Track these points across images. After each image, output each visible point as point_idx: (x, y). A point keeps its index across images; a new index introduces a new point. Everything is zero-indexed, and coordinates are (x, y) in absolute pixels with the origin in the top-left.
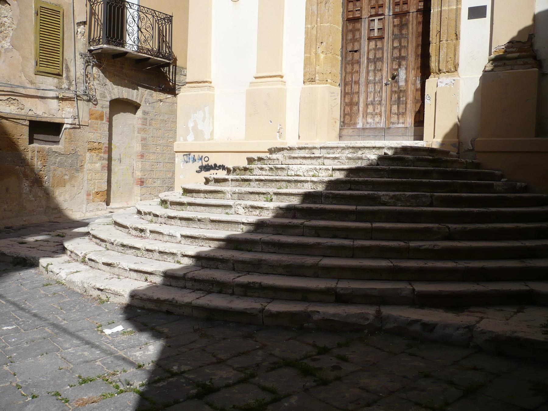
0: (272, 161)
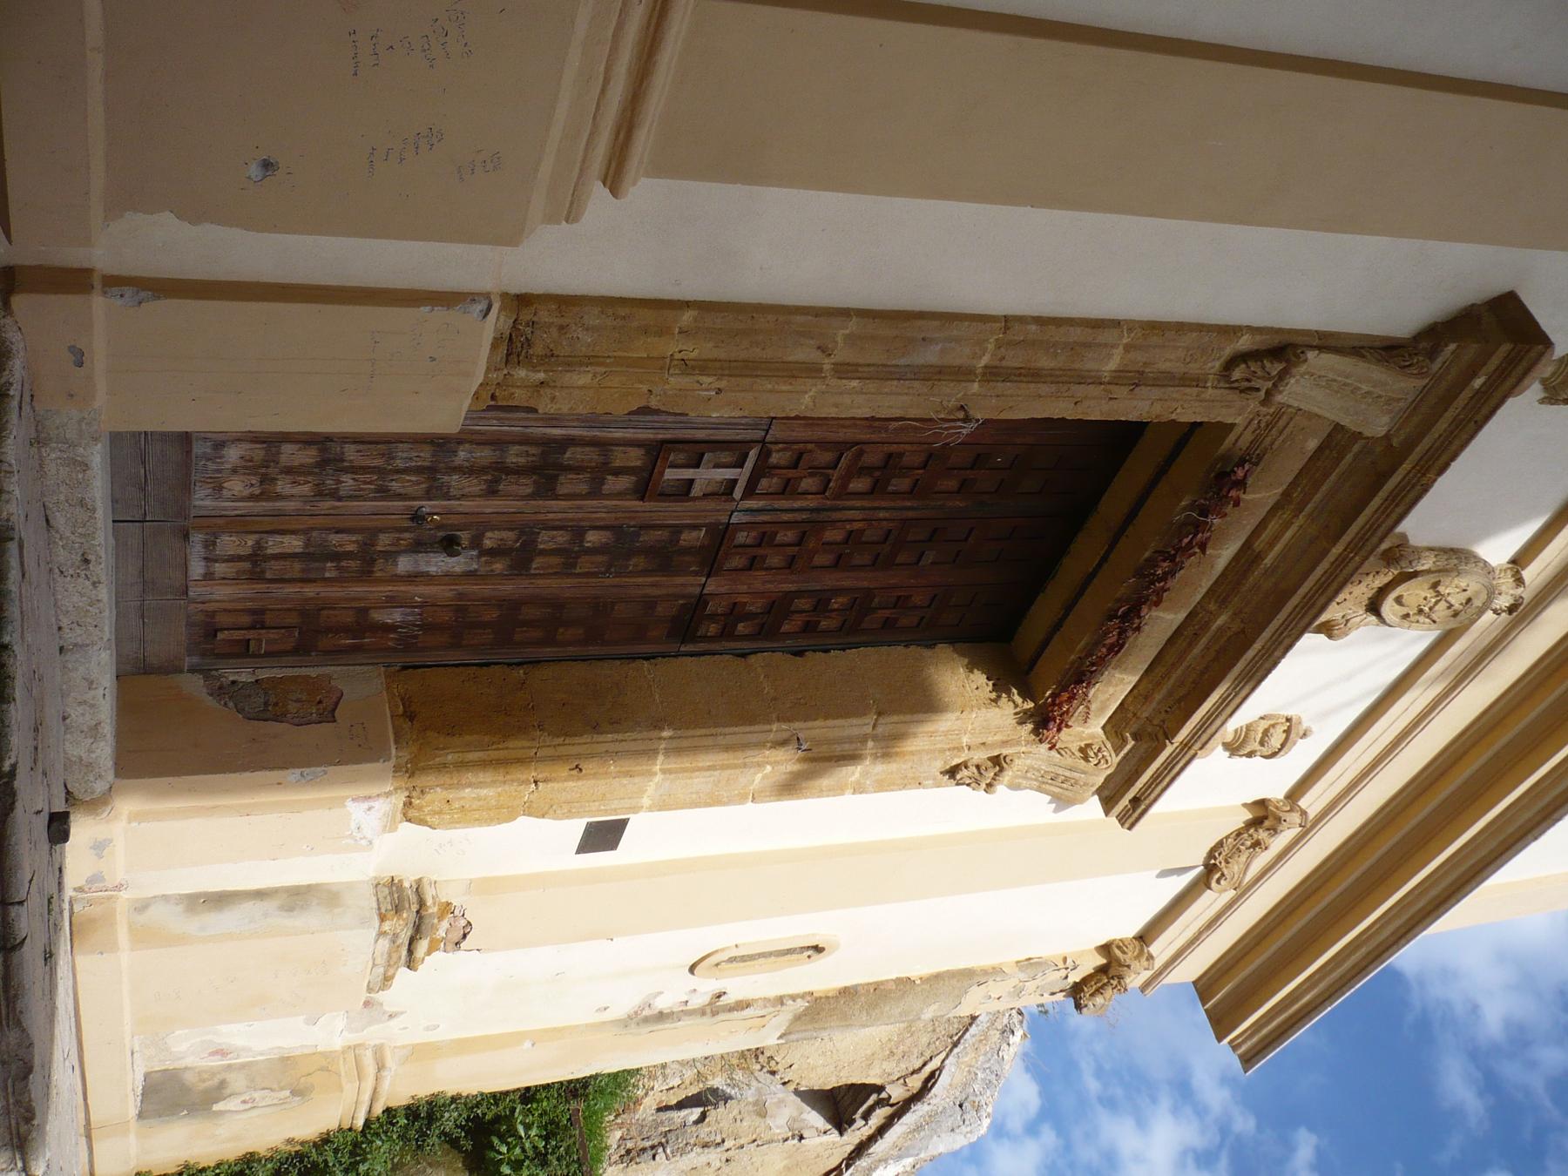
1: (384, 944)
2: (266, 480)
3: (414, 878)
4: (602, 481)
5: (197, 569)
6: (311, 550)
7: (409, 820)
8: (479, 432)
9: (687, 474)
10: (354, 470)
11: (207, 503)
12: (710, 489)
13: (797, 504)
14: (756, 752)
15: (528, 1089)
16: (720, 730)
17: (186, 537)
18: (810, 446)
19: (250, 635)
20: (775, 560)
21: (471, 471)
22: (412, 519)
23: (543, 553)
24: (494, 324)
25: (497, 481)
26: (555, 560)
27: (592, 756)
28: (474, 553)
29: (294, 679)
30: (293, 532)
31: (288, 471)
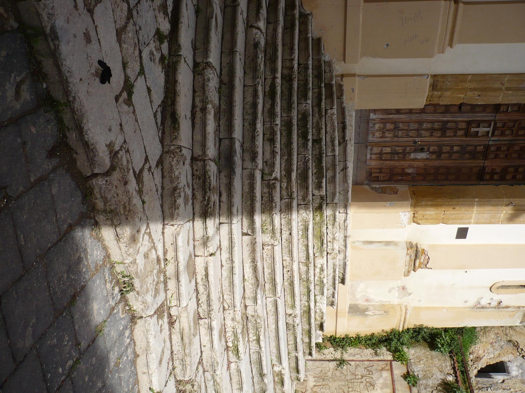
0: (331, 240)
1: (408, 257)
2: (384, 133)
3: (415, 243)
4: (457, 132)
5: (369, 156)
6: (392, 151)
7: (414, 222)
8: (428, 119)
9: (477, 129)
10: (402, 130)
11: (371, 139)
12: (483, 134)
13: (505, 138)
14: (501, 207)
15: (446, 328)
16: (491, 200)
17: (367, 147)
18: (507, 121)
19: (379, 175)
20: (502, 156)
21: (426, 130)
22: (414, 143)
23: (444, 153)
24: (428, 81)
25: (432, 132)
26: (447, 155)
27: (458, 205)
28: (428, 153)
29: (388, 187)
30: (389, 147)
31: (388, 130)
